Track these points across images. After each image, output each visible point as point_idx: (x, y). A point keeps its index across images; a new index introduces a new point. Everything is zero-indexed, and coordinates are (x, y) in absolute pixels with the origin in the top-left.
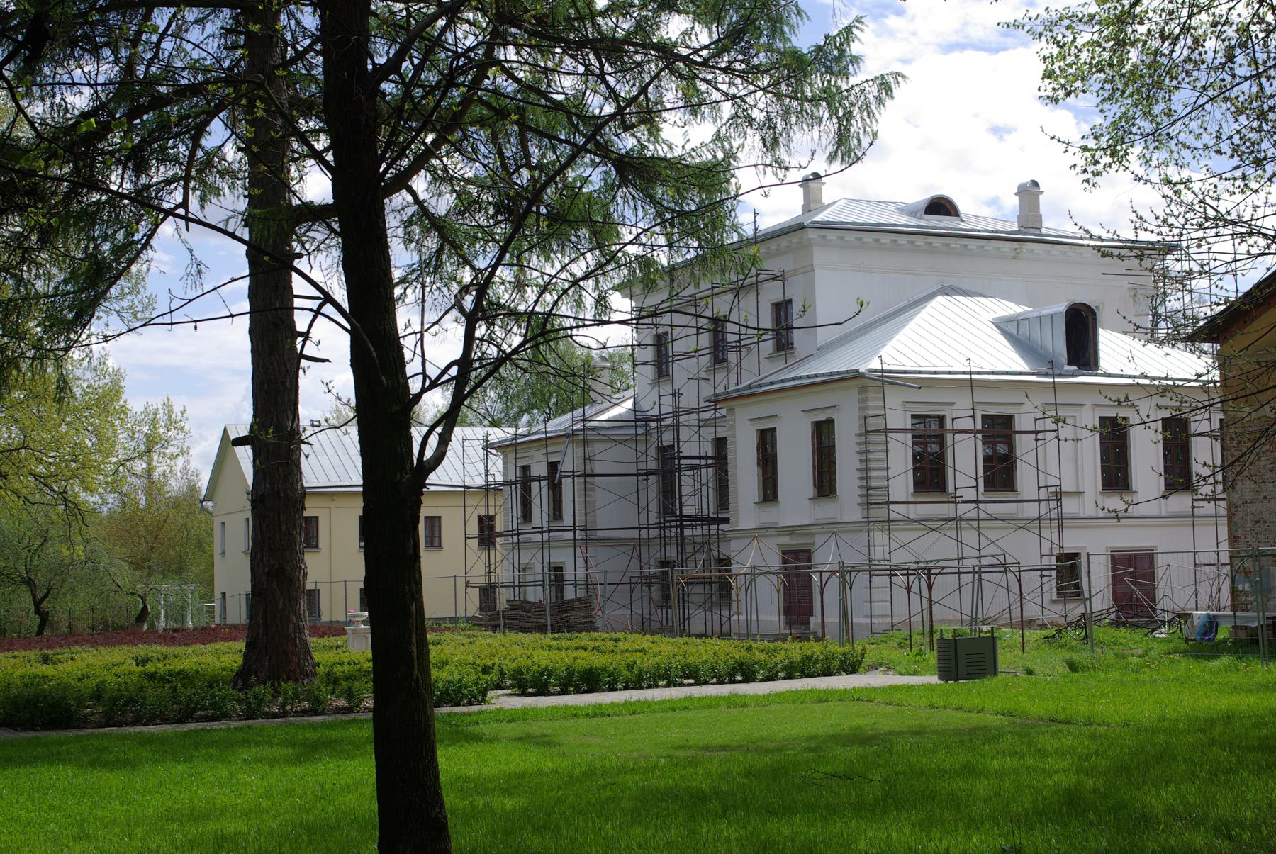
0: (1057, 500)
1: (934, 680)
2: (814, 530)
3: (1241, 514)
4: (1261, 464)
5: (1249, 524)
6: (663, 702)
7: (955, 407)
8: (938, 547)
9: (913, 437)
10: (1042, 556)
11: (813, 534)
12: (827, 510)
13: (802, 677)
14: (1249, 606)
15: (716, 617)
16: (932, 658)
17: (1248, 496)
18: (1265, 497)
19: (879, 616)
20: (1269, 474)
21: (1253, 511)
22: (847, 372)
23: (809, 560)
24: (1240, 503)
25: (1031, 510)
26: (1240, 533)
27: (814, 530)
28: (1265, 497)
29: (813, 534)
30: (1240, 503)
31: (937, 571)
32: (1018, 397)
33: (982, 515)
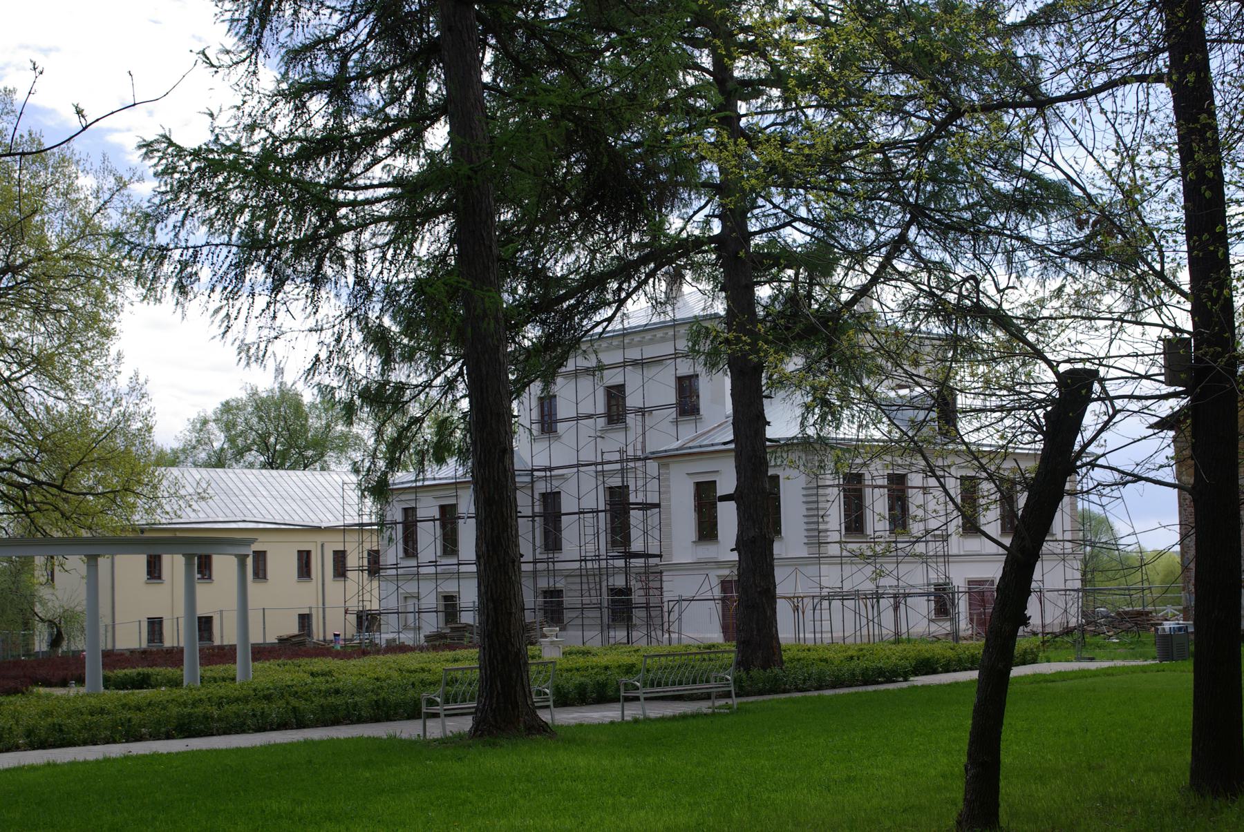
10: (1066, 581)
16: (1153, 650)
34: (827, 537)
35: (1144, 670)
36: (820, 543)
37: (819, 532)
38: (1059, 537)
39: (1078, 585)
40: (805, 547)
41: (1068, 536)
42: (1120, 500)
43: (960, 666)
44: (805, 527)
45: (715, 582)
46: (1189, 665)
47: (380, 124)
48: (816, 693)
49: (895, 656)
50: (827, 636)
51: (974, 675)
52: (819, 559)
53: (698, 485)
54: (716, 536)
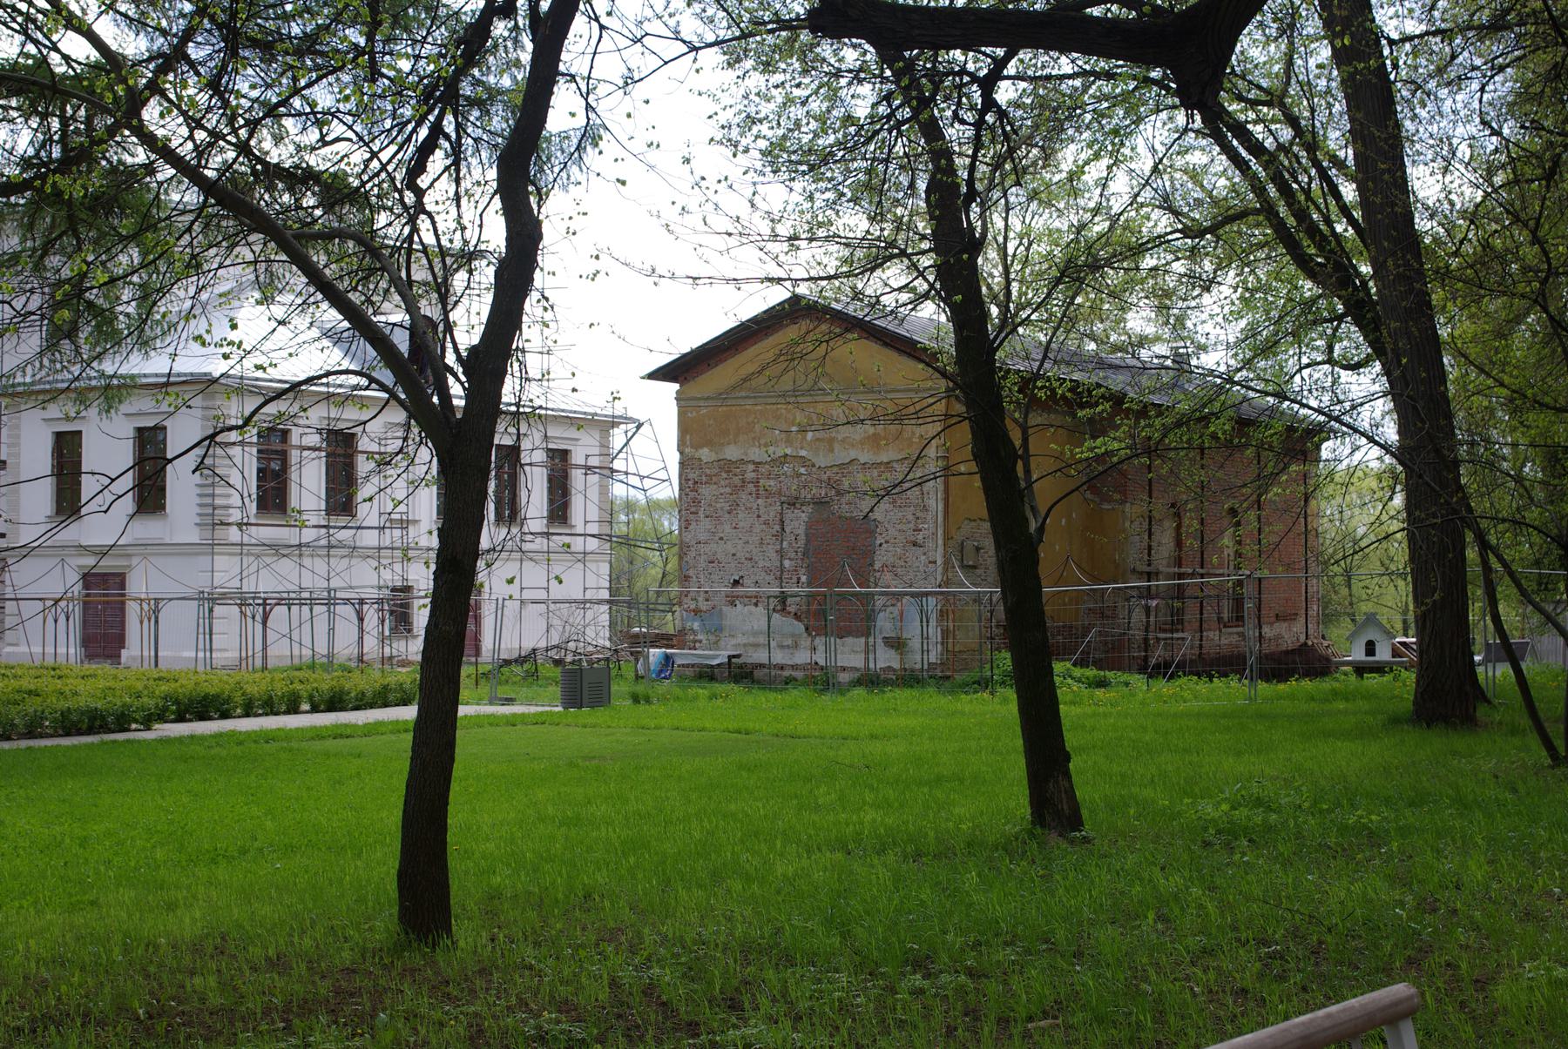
0: (402, 528)
1: (560, 709)
2: (130, 550)
3: (693, 554)
4: (718, 505)
5: (702, 564)
6: (489, 716)
7: (580, 443)
8: (269, 579)
9: (259, 451)
10: (585, 589)
11: (129, 556)
12: (148, 529)
13: (267, 715)
14: (697, 645)
15: (50, 650)
16: (556, 690)
17: (702, 537)
18: (721, 539)
19: (220, 650)
20: (727, 516)
21: (707, 550)
22: (192, 374)
23: (122, 586)
24: (693, 543)
25: (369, 539)
26: (691, 573)
27: (130, 550)
28: (721, 539)
29: (129, 556)
30: (693, 543)
31: (273, 602)
32: (573, 433)
33: (333, 542)
34: (229, 515)
35: (538, 720)
36: (214, 524)
37: (214, 509)
38: (579, 530)
39: (605, 595)
40: (197, 530)
41: (593, 529)
42: (667, 483)
43: (382, 699)
44: (198, 501)
45: (73, 577)
46: (1011, 694)
47: (1273, 121)
48: (24, 744)
49: (256, 687)
50: (307, 652)
51: (410, 713)
52: (211, 547)
53: (140, 430)
54: (163, 507)
